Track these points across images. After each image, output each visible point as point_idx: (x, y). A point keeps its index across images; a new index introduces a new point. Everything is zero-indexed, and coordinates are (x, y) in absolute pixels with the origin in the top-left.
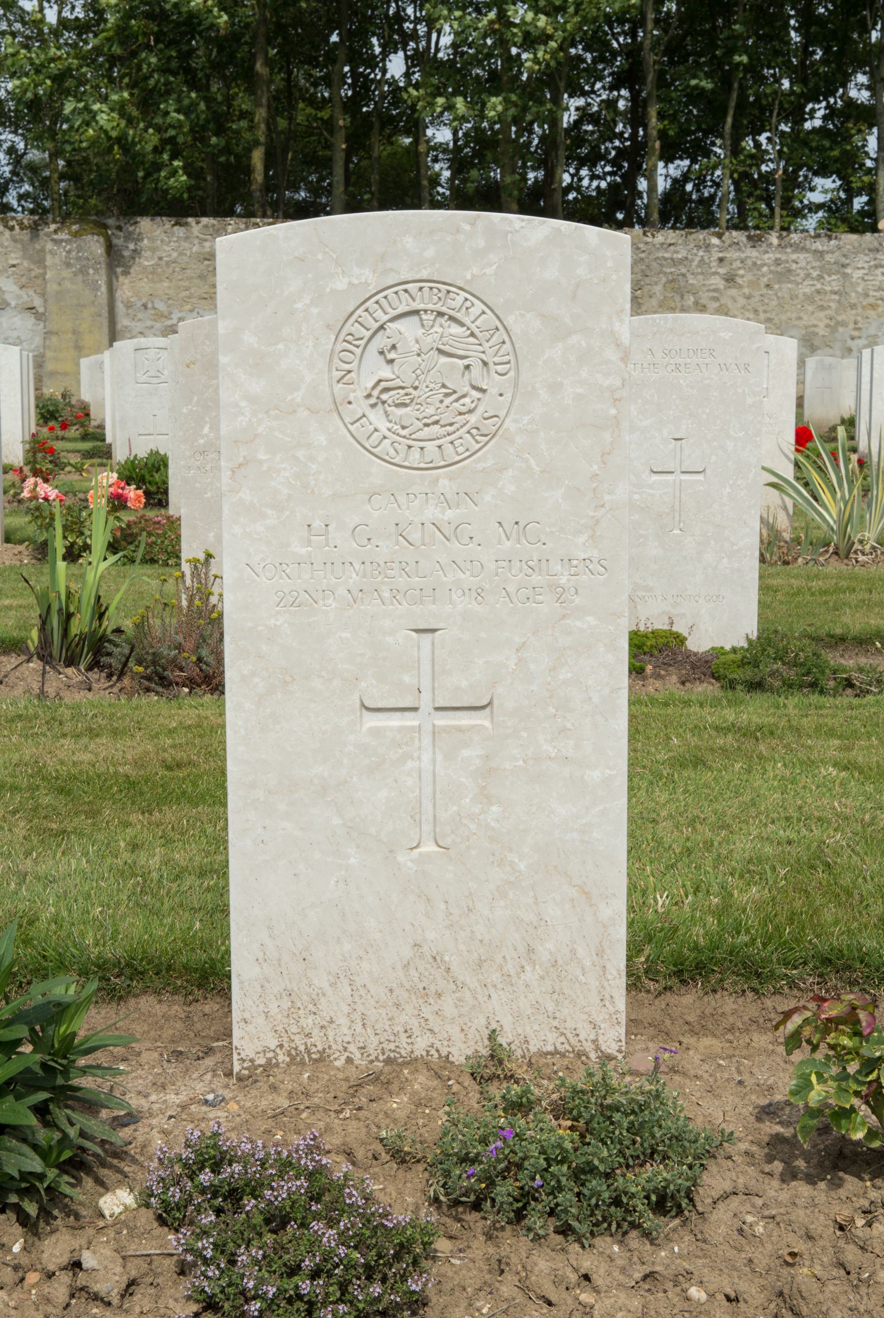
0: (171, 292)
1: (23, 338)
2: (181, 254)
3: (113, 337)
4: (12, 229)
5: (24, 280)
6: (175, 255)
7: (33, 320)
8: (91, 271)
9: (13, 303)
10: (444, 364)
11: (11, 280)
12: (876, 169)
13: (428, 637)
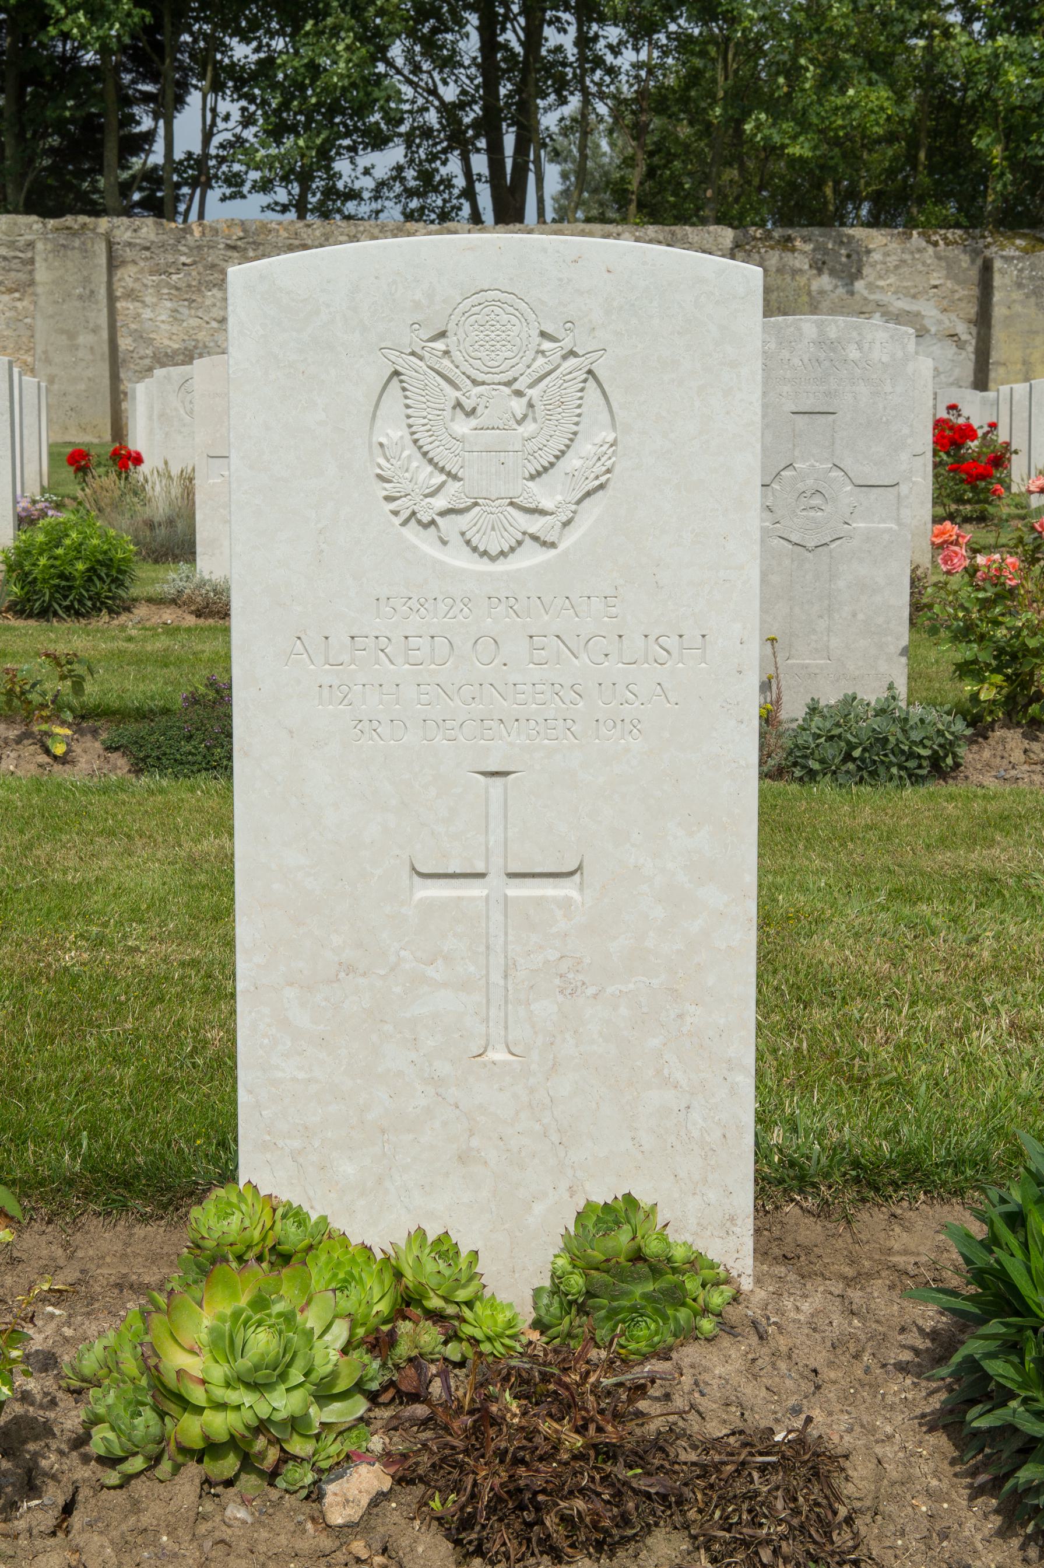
1: (941, 369)
4: (935, 244)
5: (945, 303)
7: (954, 349)
9: (933, 330)
11: (932, 302)
13: (499, 781)
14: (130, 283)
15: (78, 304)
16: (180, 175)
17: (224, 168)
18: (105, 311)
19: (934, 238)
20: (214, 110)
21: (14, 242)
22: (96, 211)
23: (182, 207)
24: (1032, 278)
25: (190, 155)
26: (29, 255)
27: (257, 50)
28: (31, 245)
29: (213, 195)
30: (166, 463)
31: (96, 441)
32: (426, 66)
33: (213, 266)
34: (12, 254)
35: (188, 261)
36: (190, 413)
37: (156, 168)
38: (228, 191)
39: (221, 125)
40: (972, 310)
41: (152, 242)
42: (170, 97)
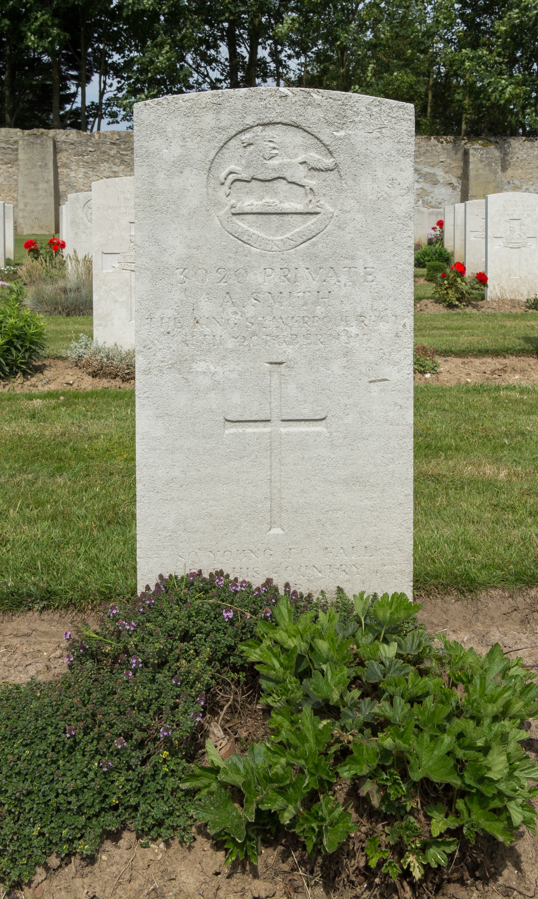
0: (523, 175)
2: (528, 156)
3: (465, 197)
4: (442, 143)
6: (525, 156)
8: (493, 164)
9: (441, 181)
11: (441, 169)
12: (260, 2)
14: (64, 160)
15: (39, 169)
16: (88, 112)
17: (109, 109)
18: (52, 172)
19: (441, 140)
20: (105, 83)
21: (8, 141)
22: (48, 127)
23: (89, 127)
24: (487, 158)
25: (93, 103)
26: (16, 147)
27: (123, 57)
28: (16, 142)
29: (105, 121)
30: (75, 252)
31: (47, 233)
32: (203, 64)
33: (104, 152)
34: (7, 146)
35: (92, 150)
36: (90, 221)
37: (77, 108)
38: (111, 120)
39: (108, 89)
40: (460, 172)
41: (75, 141)
42: (84, 79)
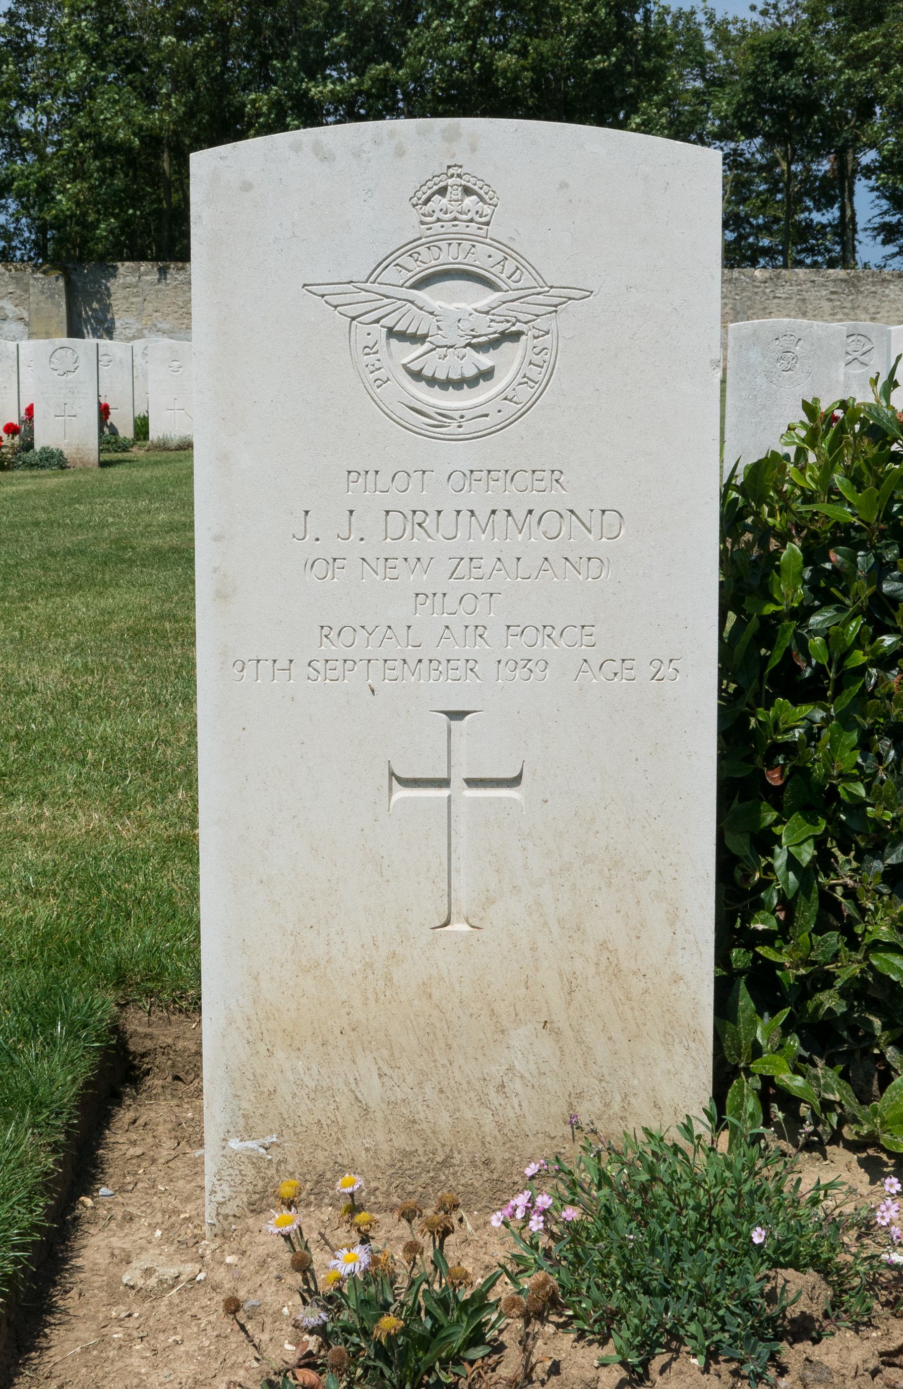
4: (10, 271)
10: (403, 801)
